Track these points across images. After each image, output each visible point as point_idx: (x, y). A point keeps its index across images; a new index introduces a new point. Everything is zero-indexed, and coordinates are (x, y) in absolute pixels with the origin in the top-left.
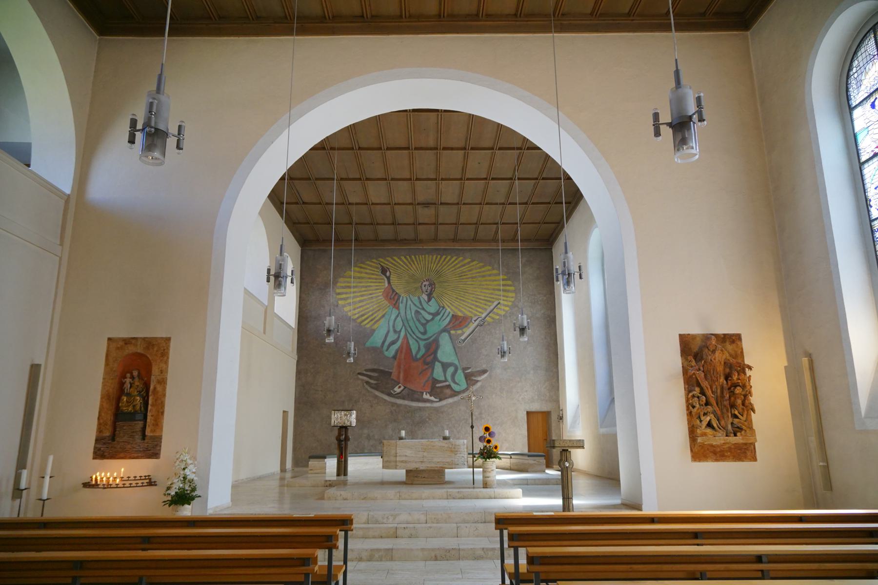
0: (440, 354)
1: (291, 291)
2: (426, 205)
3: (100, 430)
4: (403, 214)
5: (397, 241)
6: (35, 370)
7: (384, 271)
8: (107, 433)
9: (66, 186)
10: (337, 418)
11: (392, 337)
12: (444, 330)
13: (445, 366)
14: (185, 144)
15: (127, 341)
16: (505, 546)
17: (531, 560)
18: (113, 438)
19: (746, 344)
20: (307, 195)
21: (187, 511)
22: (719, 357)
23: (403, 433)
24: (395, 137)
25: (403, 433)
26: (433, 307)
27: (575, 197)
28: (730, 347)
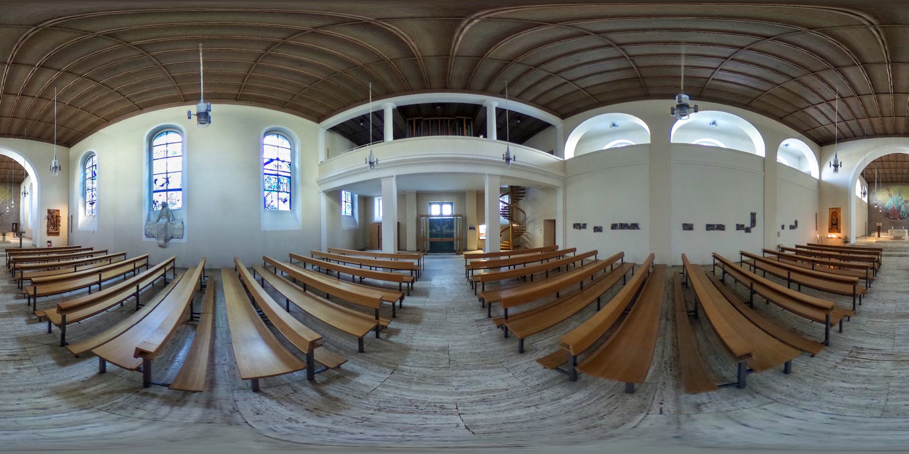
0: (901, 209)
1: (866, 196)
2: (900, 174)
3: (829, 227)
4: (894, 176)
5: (892, 182)
6: (816, 214)
7: (888, 189)
8: (830, 228)
9: (818, 178)
10: (878, 224)
11: (890, 205)
12: (903, 203)
13: (903, 212)
14: (61, 169)
15: (833, 209)
16: (501, 257)
17: (471, 263)
18: (832, 228)
19: (60, 212)
20: (869, 172)
21: (847, 245)
22: (55, 214)
23: (893, 228)
24: (891, 159)
25: (893, 228)
26: (900, 198)
27: (27, 174)
28: (57, 212)
